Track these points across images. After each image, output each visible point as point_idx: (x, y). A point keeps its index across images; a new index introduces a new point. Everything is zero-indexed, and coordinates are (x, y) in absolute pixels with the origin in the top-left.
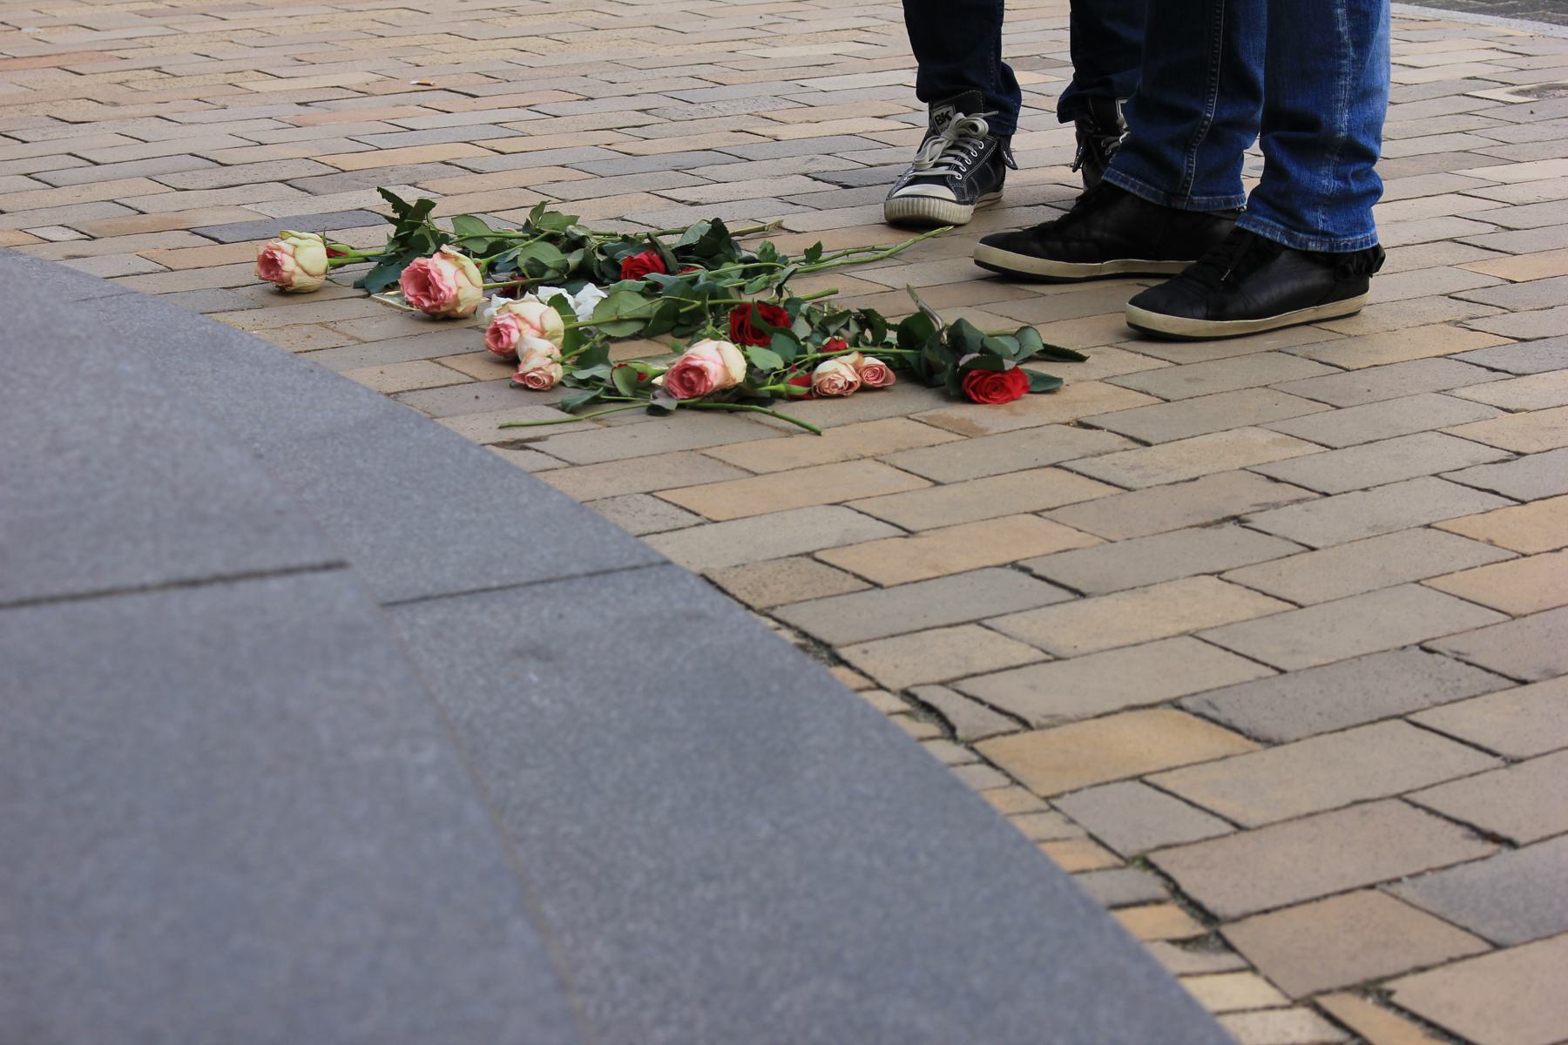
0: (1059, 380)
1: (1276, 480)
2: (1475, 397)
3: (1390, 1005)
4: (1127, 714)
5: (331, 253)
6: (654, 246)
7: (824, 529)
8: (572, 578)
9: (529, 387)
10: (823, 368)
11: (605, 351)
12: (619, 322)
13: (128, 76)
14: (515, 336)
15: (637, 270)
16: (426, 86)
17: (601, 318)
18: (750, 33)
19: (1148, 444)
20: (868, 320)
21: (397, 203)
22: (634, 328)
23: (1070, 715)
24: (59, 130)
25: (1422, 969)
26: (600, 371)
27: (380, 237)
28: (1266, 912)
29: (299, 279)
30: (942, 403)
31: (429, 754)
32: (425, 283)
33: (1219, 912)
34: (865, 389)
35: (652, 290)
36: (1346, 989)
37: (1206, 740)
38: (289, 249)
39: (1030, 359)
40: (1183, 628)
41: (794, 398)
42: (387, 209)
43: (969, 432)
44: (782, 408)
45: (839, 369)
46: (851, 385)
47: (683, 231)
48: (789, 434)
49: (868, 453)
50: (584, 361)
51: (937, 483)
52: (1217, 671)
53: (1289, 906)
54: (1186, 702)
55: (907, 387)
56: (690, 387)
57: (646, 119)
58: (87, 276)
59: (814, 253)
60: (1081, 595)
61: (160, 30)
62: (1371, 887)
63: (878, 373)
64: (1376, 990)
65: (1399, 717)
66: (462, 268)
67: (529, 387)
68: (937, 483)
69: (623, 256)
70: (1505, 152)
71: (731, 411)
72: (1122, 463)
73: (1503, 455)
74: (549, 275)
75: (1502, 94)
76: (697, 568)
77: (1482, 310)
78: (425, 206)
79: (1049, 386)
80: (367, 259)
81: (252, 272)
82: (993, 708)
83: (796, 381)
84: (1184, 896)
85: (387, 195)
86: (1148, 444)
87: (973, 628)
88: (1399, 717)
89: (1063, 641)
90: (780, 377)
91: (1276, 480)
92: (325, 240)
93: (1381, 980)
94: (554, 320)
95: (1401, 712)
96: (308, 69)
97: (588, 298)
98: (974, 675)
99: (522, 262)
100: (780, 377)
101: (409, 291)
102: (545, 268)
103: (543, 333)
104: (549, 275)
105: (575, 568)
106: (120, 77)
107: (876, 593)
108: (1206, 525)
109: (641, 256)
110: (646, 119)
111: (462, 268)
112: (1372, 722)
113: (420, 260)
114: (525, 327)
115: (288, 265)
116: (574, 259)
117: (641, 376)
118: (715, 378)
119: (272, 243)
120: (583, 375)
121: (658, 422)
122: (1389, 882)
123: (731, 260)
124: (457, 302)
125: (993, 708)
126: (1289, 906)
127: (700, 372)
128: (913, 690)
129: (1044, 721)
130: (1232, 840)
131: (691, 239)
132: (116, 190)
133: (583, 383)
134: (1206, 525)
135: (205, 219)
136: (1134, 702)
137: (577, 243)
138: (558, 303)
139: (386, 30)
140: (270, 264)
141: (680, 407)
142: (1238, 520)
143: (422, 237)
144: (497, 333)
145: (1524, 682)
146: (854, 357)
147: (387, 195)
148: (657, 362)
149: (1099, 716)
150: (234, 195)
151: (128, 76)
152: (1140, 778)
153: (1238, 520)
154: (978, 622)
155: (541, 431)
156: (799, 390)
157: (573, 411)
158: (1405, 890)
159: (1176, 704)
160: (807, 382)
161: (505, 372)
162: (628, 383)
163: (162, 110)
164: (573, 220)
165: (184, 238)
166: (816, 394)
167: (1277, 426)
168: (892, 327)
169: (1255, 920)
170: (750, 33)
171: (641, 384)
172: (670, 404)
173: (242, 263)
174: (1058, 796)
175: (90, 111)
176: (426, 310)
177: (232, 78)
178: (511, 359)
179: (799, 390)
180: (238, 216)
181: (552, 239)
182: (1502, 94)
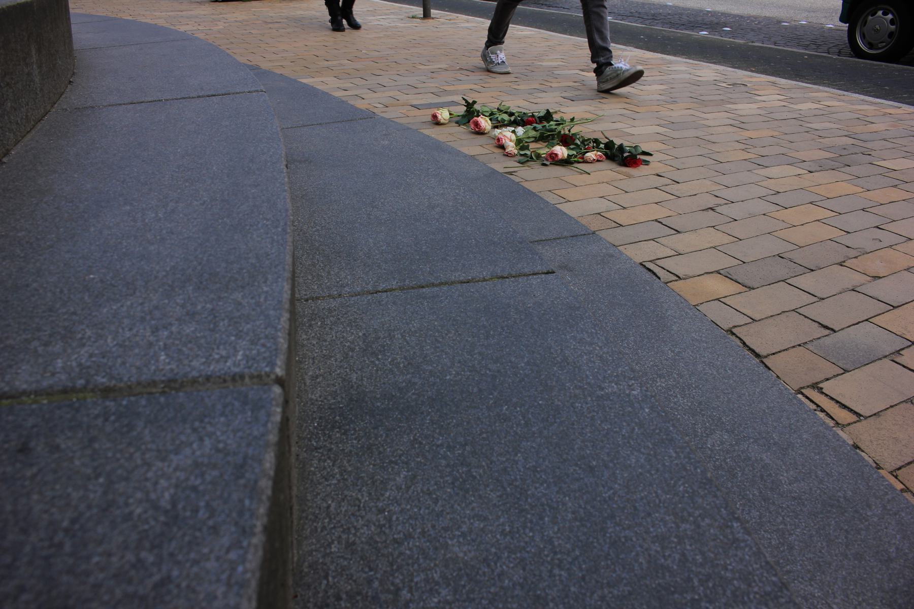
0: (649, 162)
1: (717, 197)
2: (759, 173)
3: (823, 393)
4: (706, 275)
5: (450, 114)
6: (533, 116)
7: (602, 206)
8: (566, 238)
9: (508, 155)
10: (588, 155)
11: (528, 146)
12: (529, 138)
13: (389, 63)
14: (504, 141)
15: (530, 123)
16: (461, 69)
17: (524, 136)
18: (535, 58)
19: (679, 183)
20: (596, 141)
21: (466, 101)
22: (533, 139)
23: (691, 275)
24: (374, 77)
25: (827, 379)
26: (528, 153)
27: (462, 110)
28: (774, 354)
29: (442, 121)
30: (618, 166)
31: (451, 204)
32: (477, 124)
33: (761, 354)
34: (598, 161)
35: (535, 129)
36: (808, 387)
37: (733, 288)
38: (440, 113)
39: (639, 154)
40: (712, 245)
41: (579, 162)
42: (464, 102)
43: (629, 176)
44: (576, 165)
45: (591, 155)
46: (594, 160)
47: (539, 112)
48: (581, 174)
49: (605, 181)
50: (522, 148)
51: (626, 192)
52: (725, 262)
53: (780, 352)
54: (722, 272)
55: (608, 161)
56: (553, 158)
57: (517, 80)
58: (397, 123)
59: (572, 120)
60: (678, 232)
61: (394, 52)
62: (800, 345)
63: (601, 157)
64: (815, 386)
65: (782, 281)
66: (486, 121)
67: (508, 155)
68: (626, 192)
69: (525, 119)
70: (732, 101)
71: (563, 166)
72: (674, 188)
73: (774, 193)
74: (506, 122)
75: (724, 85)
76: (639, 260)
77: (748, 147)
78: (474, 102)
79: (647, 163)
80: (459, 116)
81: (429, 118)
82: (668, 271)
83: (580, 158)
84: (748, 346)
85: (464, 99)
86: (679, 183)
87: (652, 242)
88: (782, 281)
89: (680, 248)
90: (576, 156)
91: (717, 197)
92: (449, 111)
93: (817, 383)
94: (514, 137)
95: (783, 279)
96: (432, 63)
97: (520, 130)
98: (659, 259)
99: (499, 119)
100: (576, 156)
101: (472, 126)
102: (505, 121)
103: (511, 141)
104: (506, 122)
105: (565, 234)
106: (387, 64)
107: (621, 227)
108: (703, 210)
109: (530, 119)
110: (517, 80)
111: (486, 121)
112: (776, 282)
113: (475, 118)
114: (506, 139)
115: (440, 117)
116: (512, 118)
117: (539, 154)
118: (560, 157)
119: (436, 111)
120: (522, 152)
121: (544, 168)
122: (804, 343)
123: (552, 120)
124: (485, 129)
125: (668, 271)
126: (780, 352)
127: (556, 155)
128: (643, 263)
129: (684, 277)
130: (753, 325)
131: (542, 114)
132: (391, 94)
133: (521, 155)
134: (703, 210)
135: (415, 103)
136: (707, 271)
137: (511, 114)
138: (514, 132)
139: (448, 54)
140: (435, 116)
141: (551, 164)
142: (711, 209)
143: (473, 111)
144: (499, 140)
145: (812, 270)
146: (595, 152)
147: (464, 99)
148: (544, 151)
149: (698, 276)
150: (420, 96)
151: (389, 63)
152: (718, 299)
153: (711, 209)
154: (653, 240)
155: (515, 169)
156: (581, 160)
157: (522, 163)
158: (809, 346)
159: (718, 272)
160: (583, 158)
161: (500, 151)
162: (535, 156)
163: (398, 73)
164: (509, 107)
165: (410, 108)
166: (586, 162)
167: (711, 179)
168: (603, 144)
169: (771, 357)
170: (535, 58)
171: (538, 156)
172: (548, 163)
173: (426, 115)
174: (697, 305)
175: (381, 73)
176: (477, 131)
177: (414, 65)
178: (502, 147)
179: (581, 160)
180: (423, 102)
181: (506, 113)
182: (724, 85)
